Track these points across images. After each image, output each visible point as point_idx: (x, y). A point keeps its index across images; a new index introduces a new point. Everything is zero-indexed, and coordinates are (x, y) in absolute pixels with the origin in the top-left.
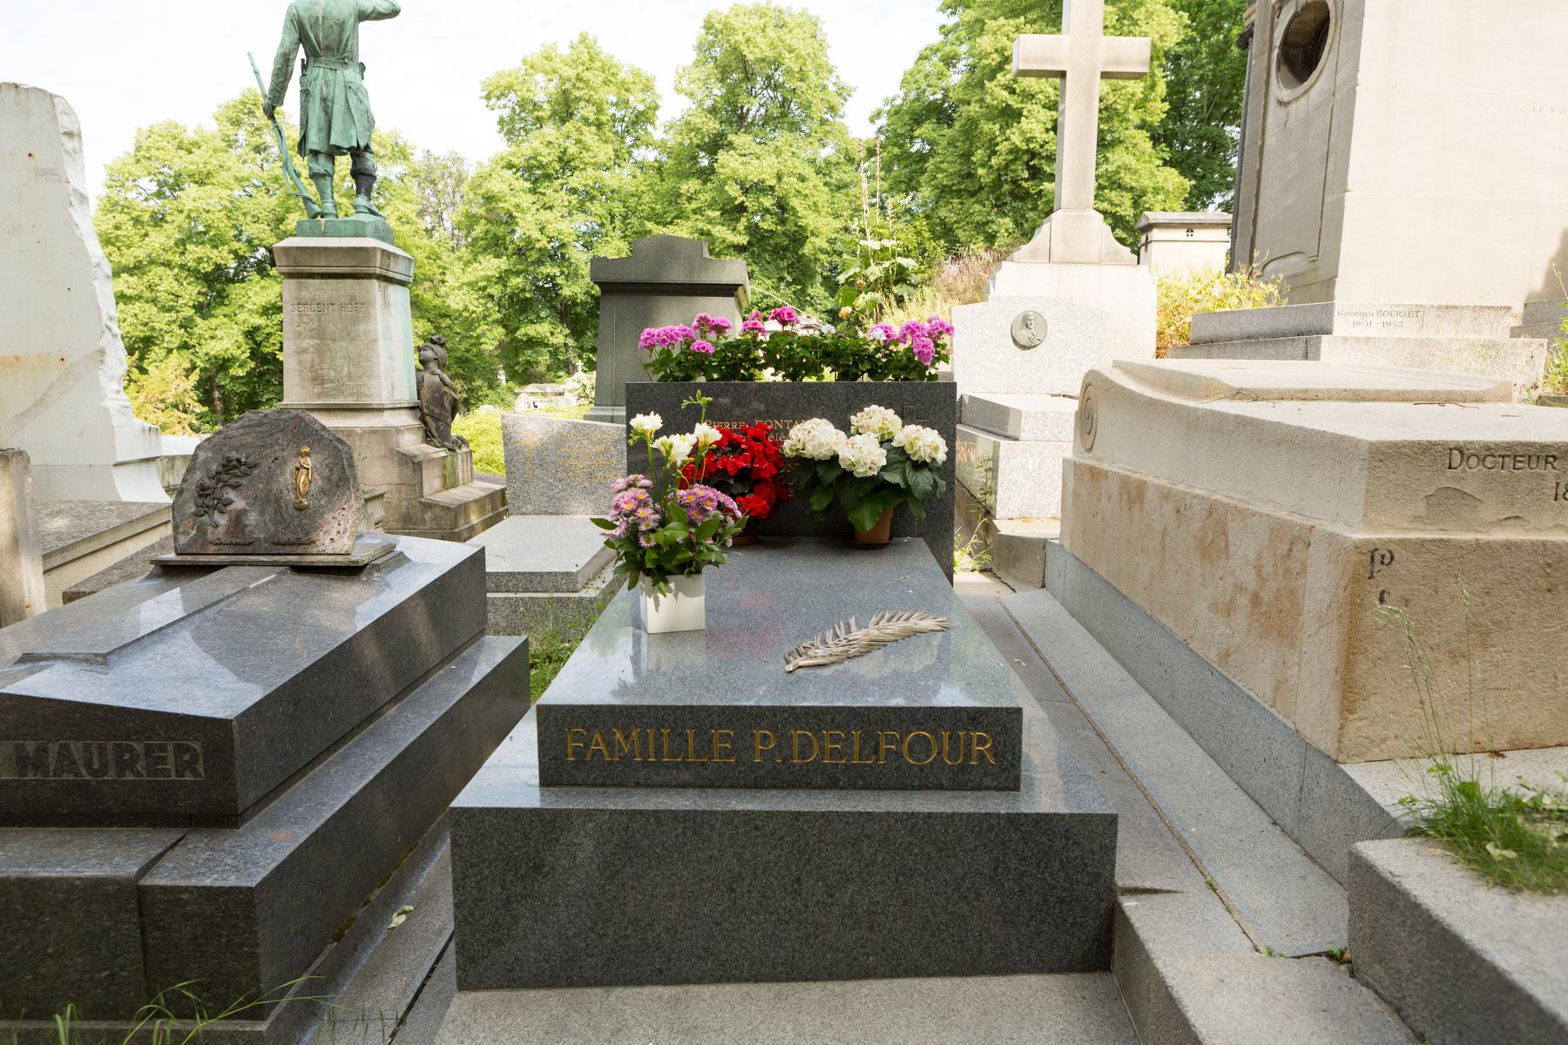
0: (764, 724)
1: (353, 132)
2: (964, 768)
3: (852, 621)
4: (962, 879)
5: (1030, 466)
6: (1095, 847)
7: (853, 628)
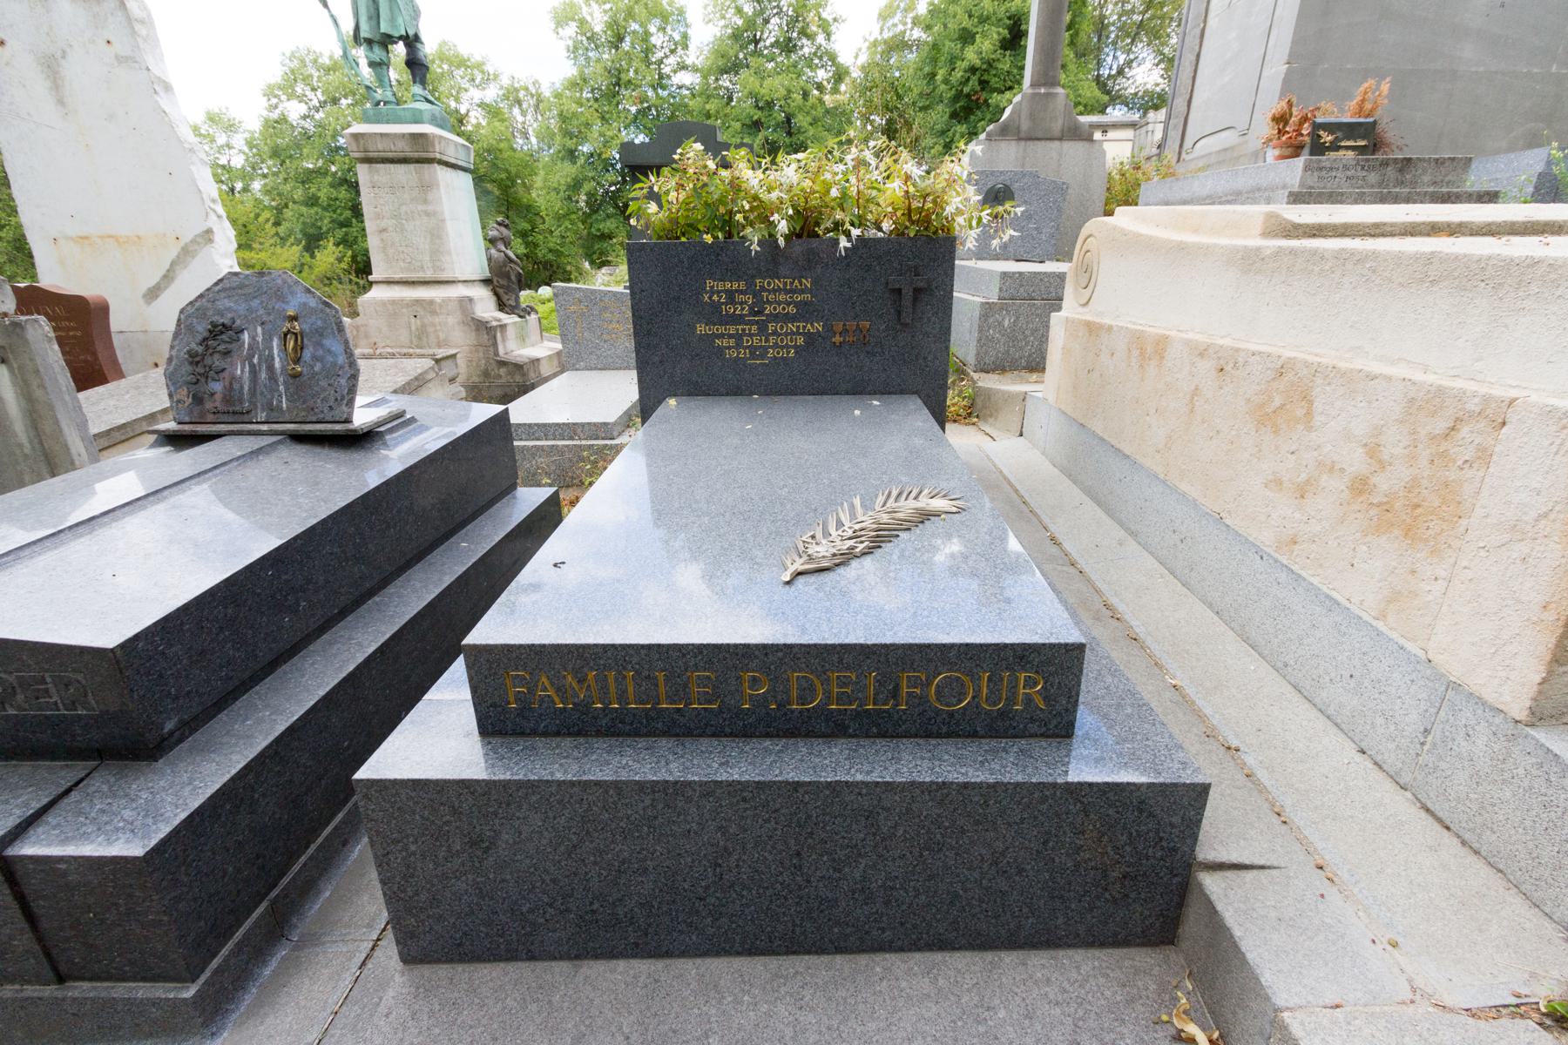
0: (753, 665)
1: (400, 21)
2: (1003, 714)
3: (857, 502)
4: (1003, 854)
5: (1006, 323)
6: (1176, 820)
7: (859, 510)
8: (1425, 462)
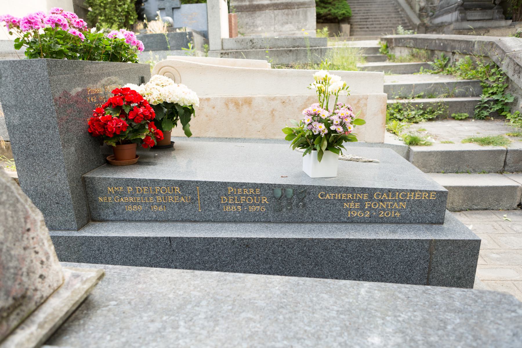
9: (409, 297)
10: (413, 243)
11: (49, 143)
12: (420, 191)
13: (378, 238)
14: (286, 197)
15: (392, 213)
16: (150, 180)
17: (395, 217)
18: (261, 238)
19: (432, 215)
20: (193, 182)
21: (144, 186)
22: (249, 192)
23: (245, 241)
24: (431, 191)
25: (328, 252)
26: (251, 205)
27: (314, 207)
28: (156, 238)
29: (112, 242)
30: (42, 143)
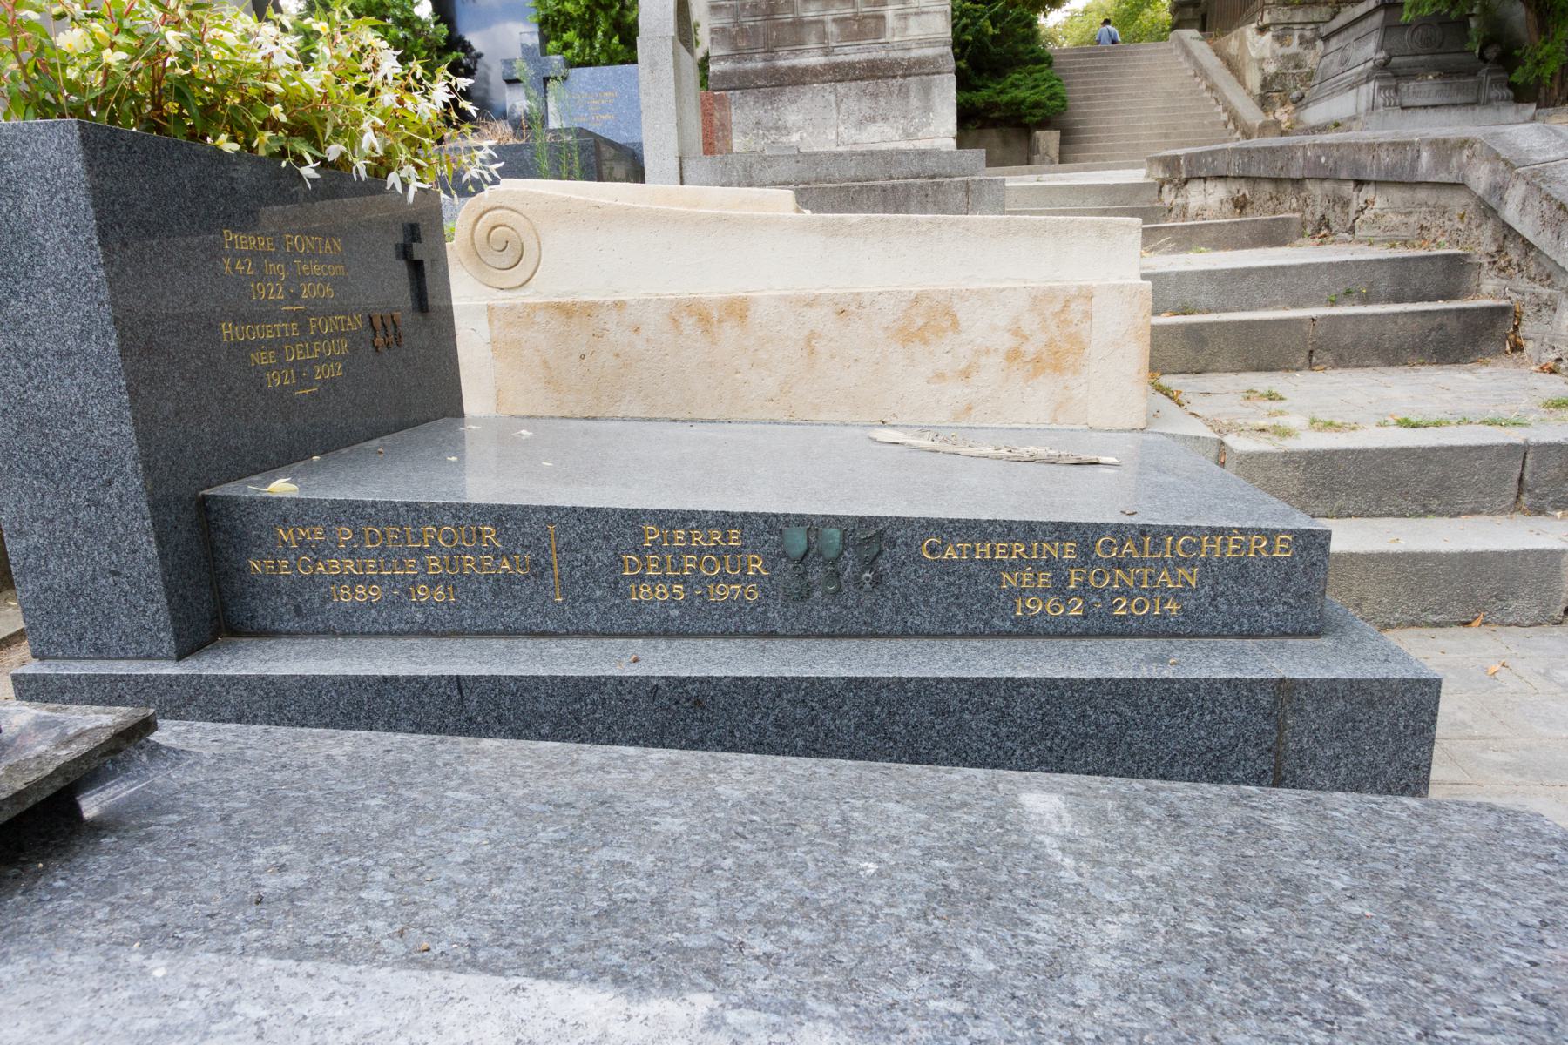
8: (1053, 328)
9: (1179, 816)
10: (1219, 692)
11: (88, 385)
12: (1242, 531)
13: (1108, 675)
14: (820, 554)
15: (1153, 604)
16: (406, 504)
17: (1164, 616)
18: (741, 679)
19: (1281, 608)
20: (535, 509)
21: (388, 523)
22: (707, 539)
23: (689, 687)
24: (1276, 532)
25: (951, 721)
26: (715, 581)
27: (907, 587)
28: (417, 679)
29: (281, 693)
30: (67, 382)
